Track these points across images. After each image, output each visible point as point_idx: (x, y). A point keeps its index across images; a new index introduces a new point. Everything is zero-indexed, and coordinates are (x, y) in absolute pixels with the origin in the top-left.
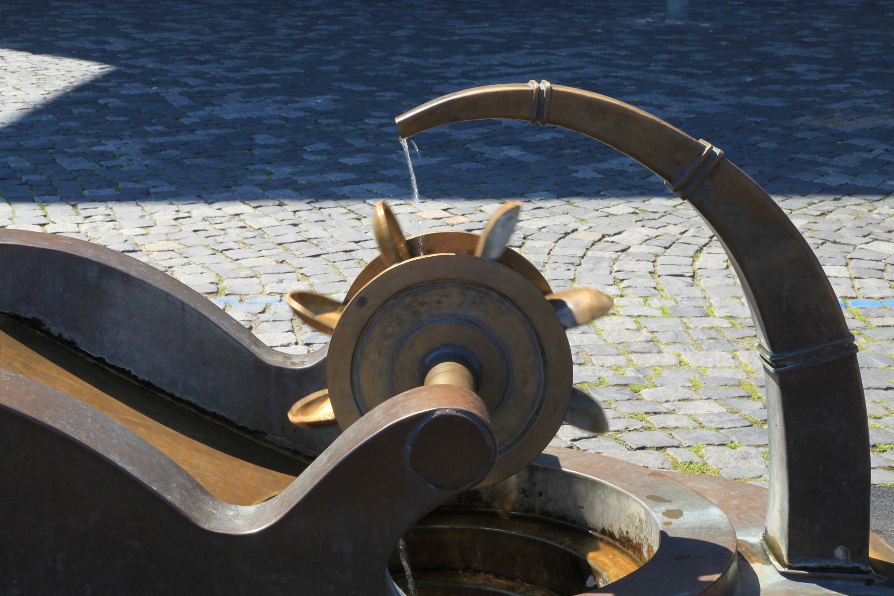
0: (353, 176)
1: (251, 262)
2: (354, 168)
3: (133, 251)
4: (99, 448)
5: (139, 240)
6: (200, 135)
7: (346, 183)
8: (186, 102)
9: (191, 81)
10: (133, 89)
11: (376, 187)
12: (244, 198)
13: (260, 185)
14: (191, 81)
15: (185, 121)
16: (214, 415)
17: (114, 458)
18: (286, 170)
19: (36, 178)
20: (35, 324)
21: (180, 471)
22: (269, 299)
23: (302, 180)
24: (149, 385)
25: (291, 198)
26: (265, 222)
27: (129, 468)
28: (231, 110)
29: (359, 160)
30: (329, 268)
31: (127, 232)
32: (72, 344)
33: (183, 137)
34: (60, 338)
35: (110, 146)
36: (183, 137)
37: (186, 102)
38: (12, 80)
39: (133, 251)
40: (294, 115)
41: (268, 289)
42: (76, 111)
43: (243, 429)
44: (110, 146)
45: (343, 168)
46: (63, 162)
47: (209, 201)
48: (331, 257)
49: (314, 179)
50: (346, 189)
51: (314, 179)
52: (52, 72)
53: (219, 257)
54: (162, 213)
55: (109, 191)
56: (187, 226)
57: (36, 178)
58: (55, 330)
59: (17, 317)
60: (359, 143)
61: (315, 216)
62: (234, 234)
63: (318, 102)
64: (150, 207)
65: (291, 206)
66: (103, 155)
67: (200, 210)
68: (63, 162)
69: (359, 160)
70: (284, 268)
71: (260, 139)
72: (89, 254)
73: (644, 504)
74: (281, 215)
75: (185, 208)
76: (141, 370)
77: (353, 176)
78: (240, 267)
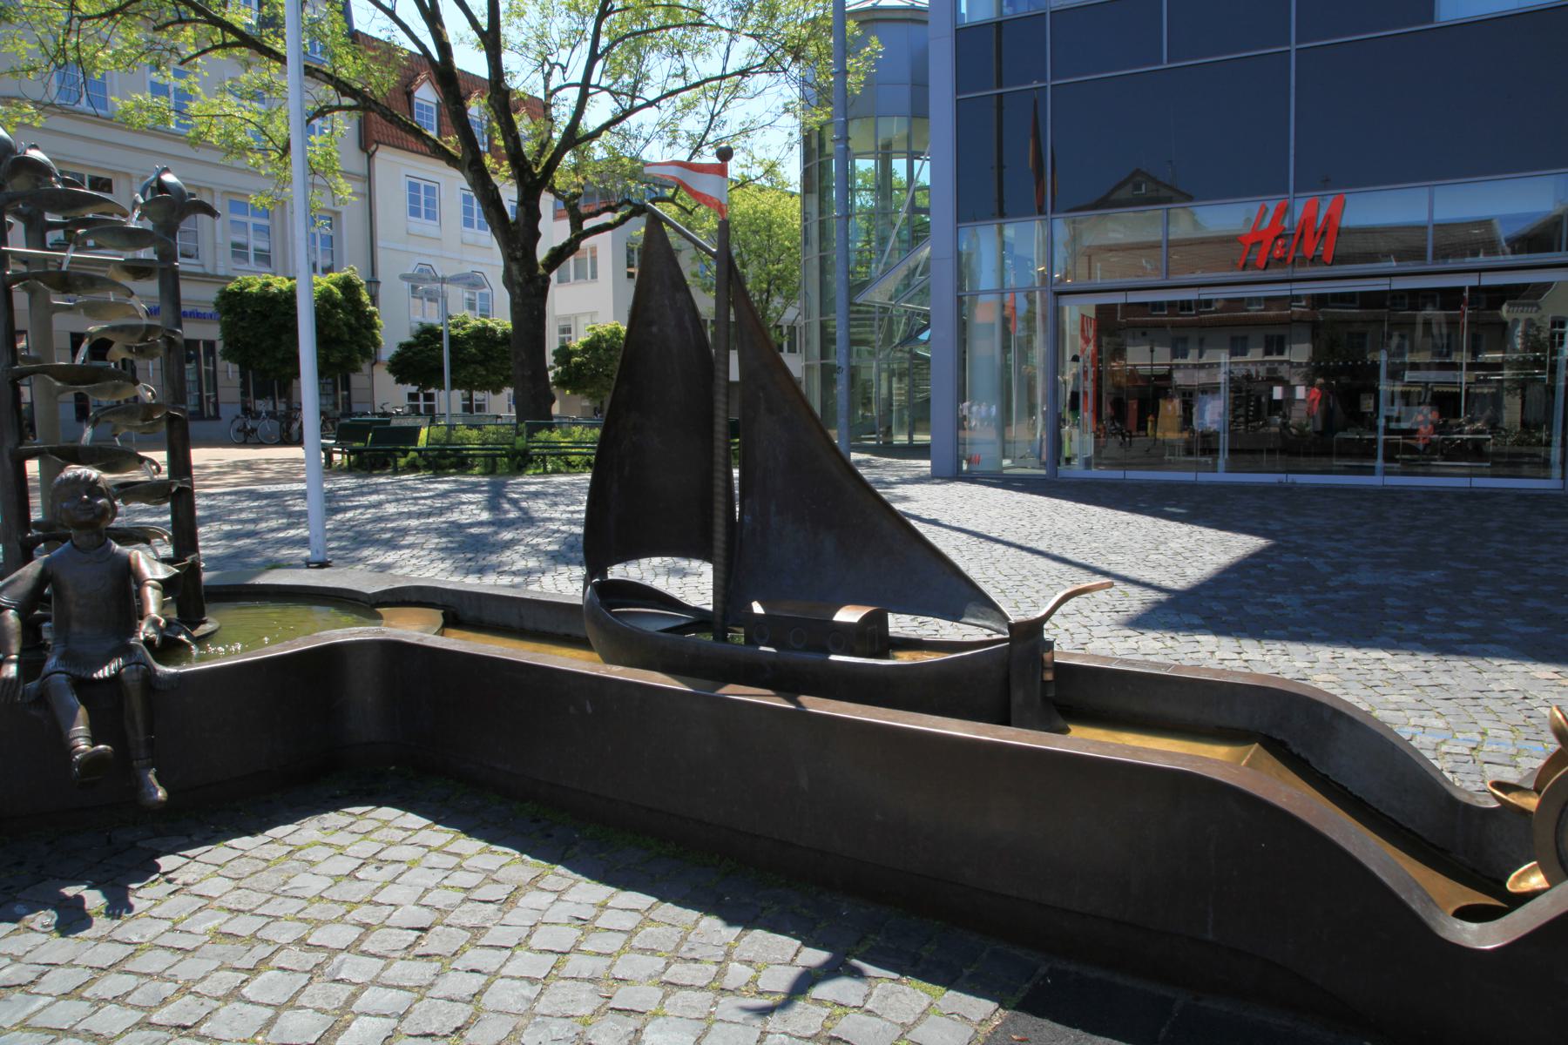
0: (1468, 637)
1: (1395, 698)
2: (1469, 631)
3: (935, 522)
4: (1363, 860)
5: (1308, 672)
6: (1343, 595)
7: (1464, 642)
8: (1330, 570)
9: (1331, 554)
10: (1289, 558)
11: (1491, 647)
12: (1384, 647)
13: (1394, 637)
14: (1331, 554)
15: (1331, 584)
16: (1409, 830)
17: (1374, 869)
18: (1413, 628)
19: (1230, 618)
20: (1282, 744)
21: (1418, 886)
22: (1415, 730)
23: (1429, 636)
24: (1360, 799)
25: (1422, 650)
26: (1403, 667)
27: (1385, 879)
28: (1364, 577)
29: (1472, 624)
30: (1460, 710)
31: (1299, 664)
32: (1307, 762)
33: (1330, 596)
34: (1298, 756)
35: (1279, 599)
36: (1330, 596)
37: (1330, 570)
38: (1208, 548)
39: (935, 522)
40: (1414, 584)
41: (1412, 722)
42: (1253, 572)
43: (1433, 845)
44: (1279, 599)
45: (1459, 630)
46: (1248, 609)
47: (1357, 647)
48: (1462, 702)
49: (1439, 636)
50: (1466, 647)
51: (1439, 636)
52: (1233, 543)
53: (1370, 692)
54: (1324, 653)
55: (1282, 633)
56: (1342, 665)
57: (1230, 618)
58: (1295, 750)
59: (1271, 738)
60: (1470, 610)
61: (1442, 666)
62: (1378, 674)
63: (1432, 575)
64: (1313, 647)
65: (1421, 657)
66: (1275, 605)
67: (1350, 653)
68: (1248, 609)
69: (1472, 624)
70: (1422, 706)
71: (1389, 601)
72: (1324, 700)
73: (987, 623)
74: (1415, 663)
75: (1339, 651)
76: (1355, 787)
77: (1468, 637)
78: (1387, 702)
